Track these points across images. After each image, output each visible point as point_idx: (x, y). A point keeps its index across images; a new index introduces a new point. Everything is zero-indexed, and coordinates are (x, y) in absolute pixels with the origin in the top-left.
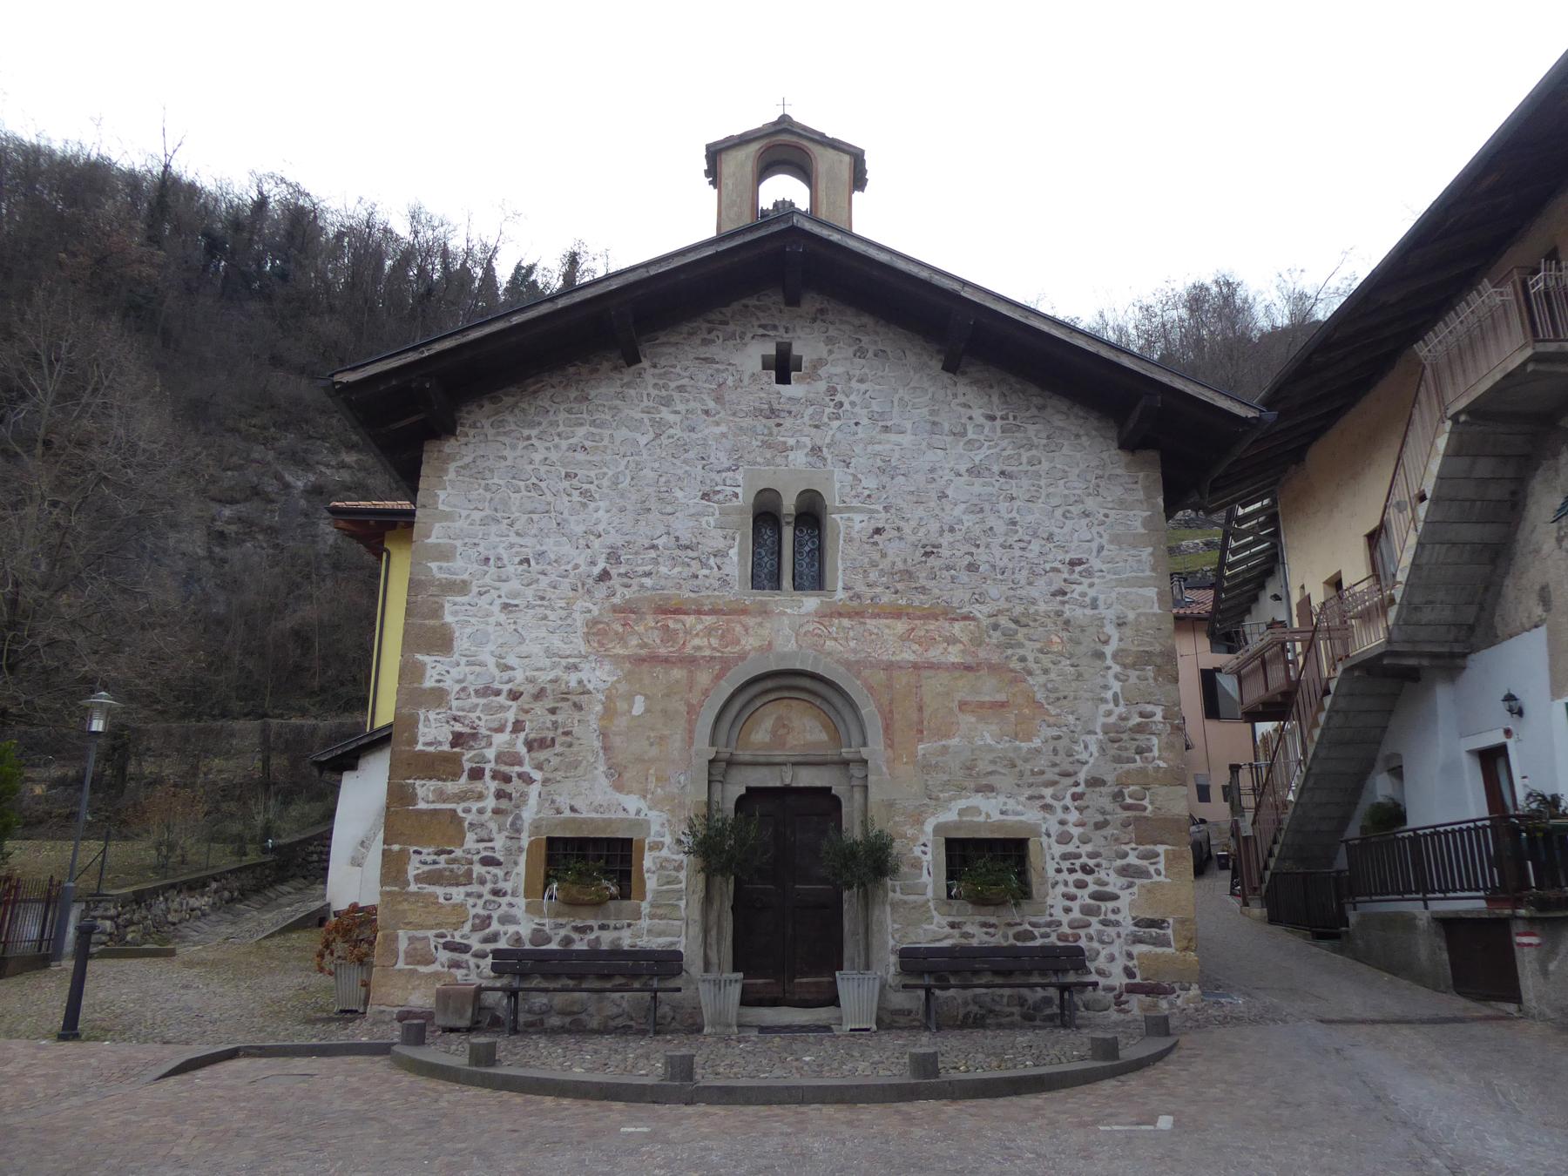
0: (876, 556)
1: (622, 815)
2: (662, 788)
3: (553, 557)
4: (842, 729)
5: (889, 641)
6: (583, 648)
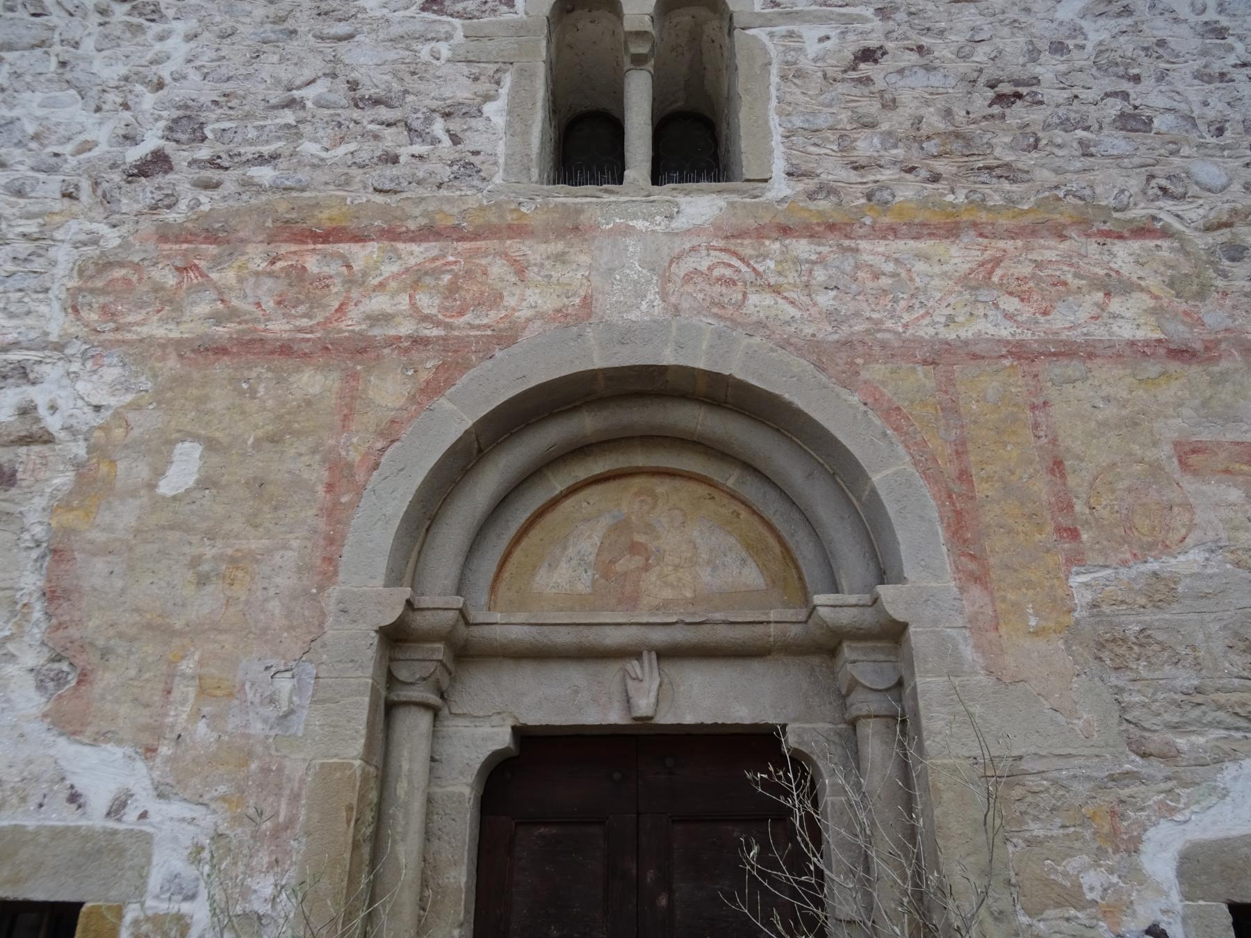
0: (871, 108)
1: (60, 816)
2: (214, 721)
3: (31, 129)
4: (806, 552)
5: (933, 290)
6: (56, 323)
